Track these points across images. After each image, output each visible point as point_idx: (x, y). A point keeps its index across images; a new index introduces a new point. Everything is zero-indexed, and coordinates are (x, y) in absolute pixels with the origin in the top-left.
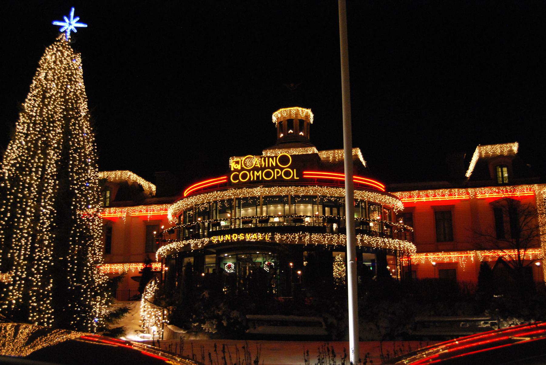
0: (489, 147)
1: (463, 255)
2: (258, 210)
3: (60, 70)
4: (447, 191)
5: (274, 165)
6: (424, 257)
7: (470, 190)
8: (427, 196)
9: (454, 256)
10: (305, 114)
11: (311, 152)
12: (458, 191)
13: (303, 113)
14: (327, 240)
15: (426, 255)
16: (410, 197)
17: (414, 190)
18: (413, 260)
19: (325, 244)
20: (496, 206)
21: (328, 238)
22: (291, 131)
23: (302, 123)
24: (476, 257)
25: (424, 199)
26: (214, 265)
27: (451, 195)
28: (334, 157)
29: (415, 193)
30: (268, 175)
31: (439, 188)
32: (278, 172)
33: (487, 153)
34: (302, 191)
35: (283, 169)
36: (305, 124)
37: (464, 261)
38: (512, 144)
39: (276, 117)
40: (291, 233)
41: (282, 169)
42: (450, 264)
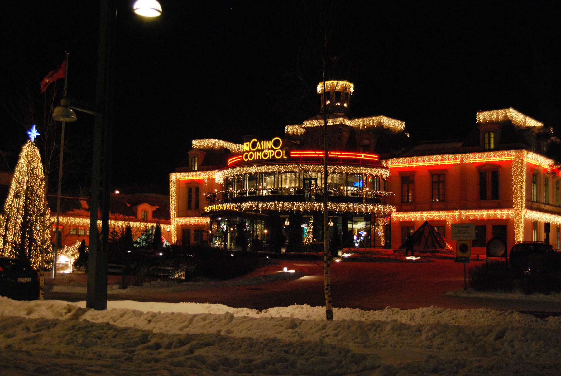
0: (487, 113)
1: (450, 214)
3: (29, 160)
4: (439, 157)
7: (458, 156)
8: (424, 161)
9: (442, 215)
17: (413, 156)
18: (395, 219)
24: (460, 216)
27: (442, 160)
37: (450, 219)
38: (506, 110)
40: (270, 201)
41: (275, 150)
42: (501, 220)
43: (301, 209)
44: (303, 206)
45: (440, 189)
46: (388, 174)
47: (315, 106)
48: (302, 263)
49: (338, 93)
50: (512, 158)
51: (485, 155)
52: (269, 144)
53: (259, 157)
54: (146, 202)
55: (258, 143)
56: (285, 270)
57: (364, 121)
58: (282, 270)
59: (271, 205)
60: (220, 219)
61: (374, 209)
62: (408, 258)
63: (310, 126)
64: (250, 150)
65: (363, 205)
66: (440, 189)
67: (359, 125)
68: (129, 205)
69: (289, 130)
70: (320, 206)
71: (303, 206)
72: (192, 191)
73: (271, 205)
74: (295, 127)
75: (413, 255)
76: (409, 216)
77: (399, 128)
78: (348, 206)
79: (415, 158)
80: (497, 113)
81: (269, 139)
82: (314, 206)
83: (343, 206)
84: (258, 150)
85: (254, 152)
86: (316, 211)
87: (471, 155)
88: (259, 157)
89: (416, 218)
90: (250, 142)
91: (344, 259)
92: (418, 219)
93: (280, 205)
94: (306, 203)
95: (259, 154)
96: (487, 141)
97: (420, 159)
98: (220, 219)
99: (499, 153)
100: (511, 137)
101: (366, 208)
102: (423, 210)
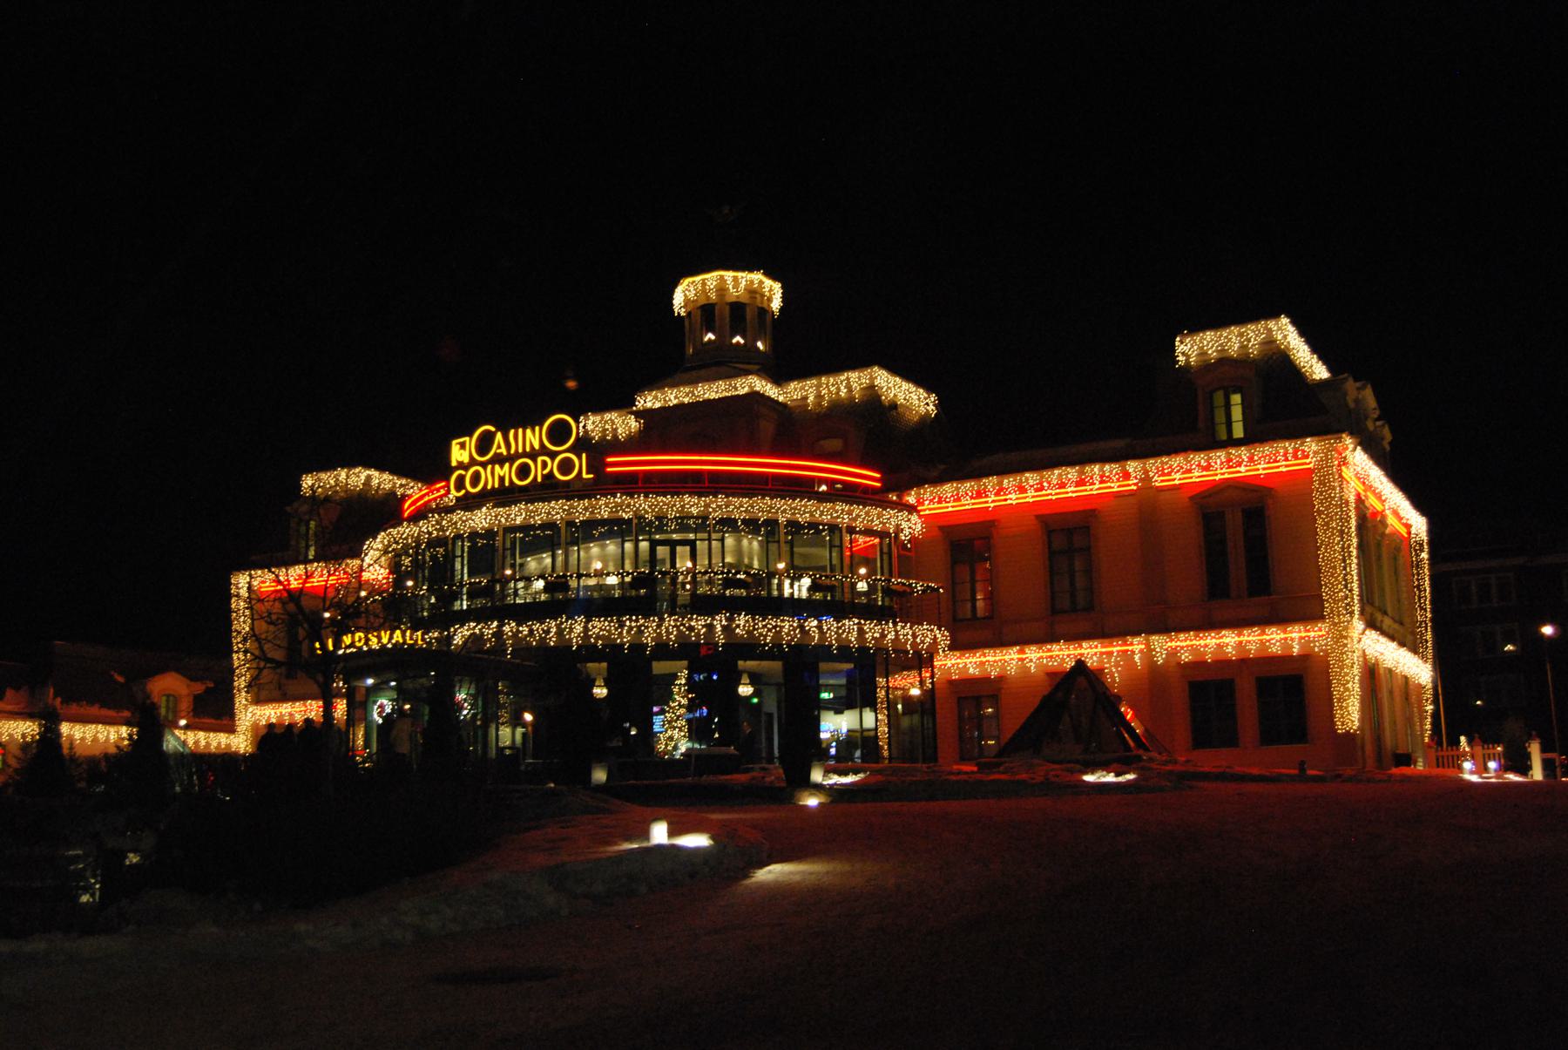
2: (628, 546)
4: (1072, 473)
5: (537, 446)
6: (1016, 656)
7: (1132, 466)
8: (1022, 490)
9: (1091, 652)
10: (743, 285)
11: (746, 390)
12: (1101, 469)
13: (736, 286)
14: (629, 632)
15: (1022, 652)
16: (979, 495)
17: (988, 475)
19: (623, 644)
20: (1212, 505)
21: (631, 628)
22: (711, 336)
23: (740, 313)
24: (1148, 653)
25: (1013, 498)
26: (843, 681)
28: (819, 397)
29: (990, 482)
30: (523, 471)
31: (1092, 460)
32: (545, 465)
33: (1203, 353)
34: (604, 507)
35: (555, 454)
36: (749, 314)
37: (1117, 665)
38: (1272, 324)
39: (683, 295)
41: (553, 455)
42: (1285, 659)
43: (648, 639)
44: (654, 630)
45: (1073, 575)
46: (919, 527)
47: (669, 349)
48: (721, 812)
49: (737, 308)
50: (1311, 463)
51: (1220, 456)
52: (533, 437)
53: (502, 479)
54: (177, 670)
55: (499, 436)
56: (659, 833)
57: (819, 386)
58: (645, 834)
59: (548, 631)
60: (370, 681)
61: (883, 636)
62: (1089, 778)
63: (658, 405)
64: (473, 462)
65: (851, 624)
66: (1073, 575)
67: (805, 398)
68: (121, 679)
69: (590, 427)
70: (710, 627)
71: (654, 630)
72: (296, 615)
73: (548, 631)
74: (607, 416)
75: (1105, 766)
76: (982, 663)
77: (922, 410)
78: (802, 627)
79: (994, 479)
80: (1241, 335)
81: (533, 421)
82: (691, 629)
83: (787, 625)
84: (499, 460)
85: (484, 465)
86: (697, 644)
87: (1177, 461)
88: (502, 479)
89: (1003, 668)
90: (471, 436)
91: (837, 793)
92: (1012, 670)
93: (576, 628)
94: (662, 620)
95: (503, 471)
96: (1220, 416)
97: (1008, 482)
98: (370, 681)
99: (1267, 449)
100: (1282, 406)
101: (861, 632)
102: (1023, 641)
